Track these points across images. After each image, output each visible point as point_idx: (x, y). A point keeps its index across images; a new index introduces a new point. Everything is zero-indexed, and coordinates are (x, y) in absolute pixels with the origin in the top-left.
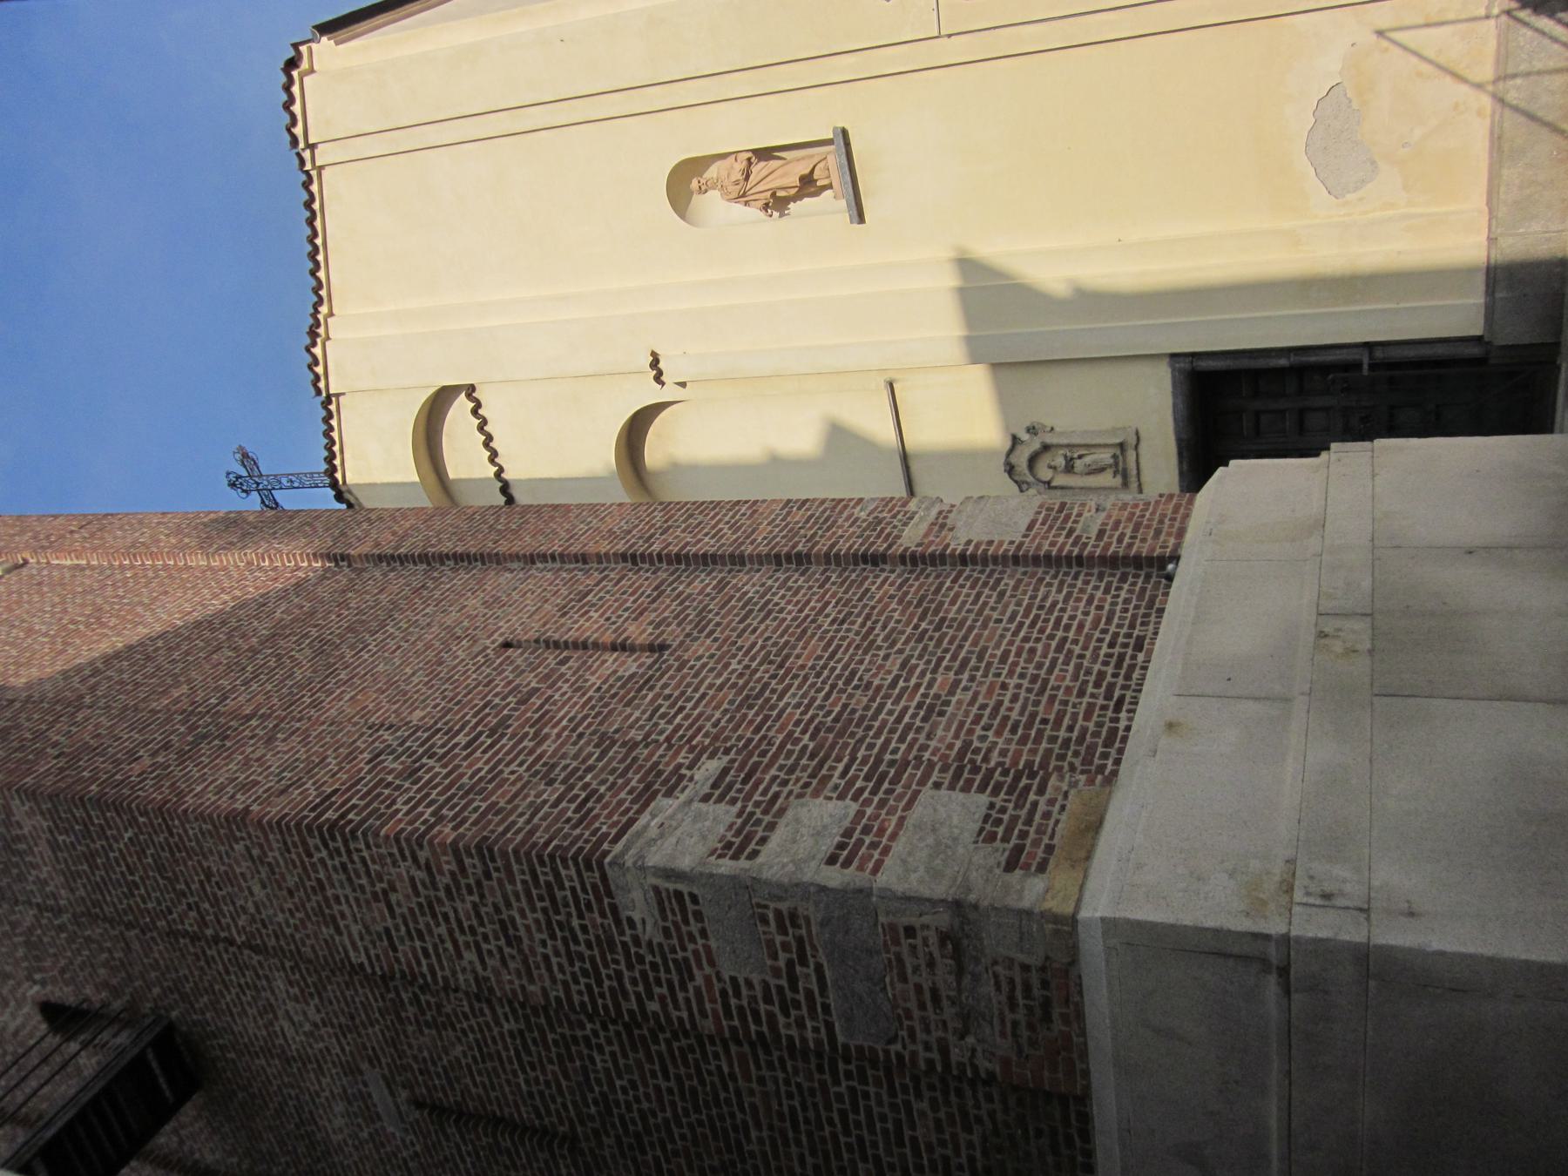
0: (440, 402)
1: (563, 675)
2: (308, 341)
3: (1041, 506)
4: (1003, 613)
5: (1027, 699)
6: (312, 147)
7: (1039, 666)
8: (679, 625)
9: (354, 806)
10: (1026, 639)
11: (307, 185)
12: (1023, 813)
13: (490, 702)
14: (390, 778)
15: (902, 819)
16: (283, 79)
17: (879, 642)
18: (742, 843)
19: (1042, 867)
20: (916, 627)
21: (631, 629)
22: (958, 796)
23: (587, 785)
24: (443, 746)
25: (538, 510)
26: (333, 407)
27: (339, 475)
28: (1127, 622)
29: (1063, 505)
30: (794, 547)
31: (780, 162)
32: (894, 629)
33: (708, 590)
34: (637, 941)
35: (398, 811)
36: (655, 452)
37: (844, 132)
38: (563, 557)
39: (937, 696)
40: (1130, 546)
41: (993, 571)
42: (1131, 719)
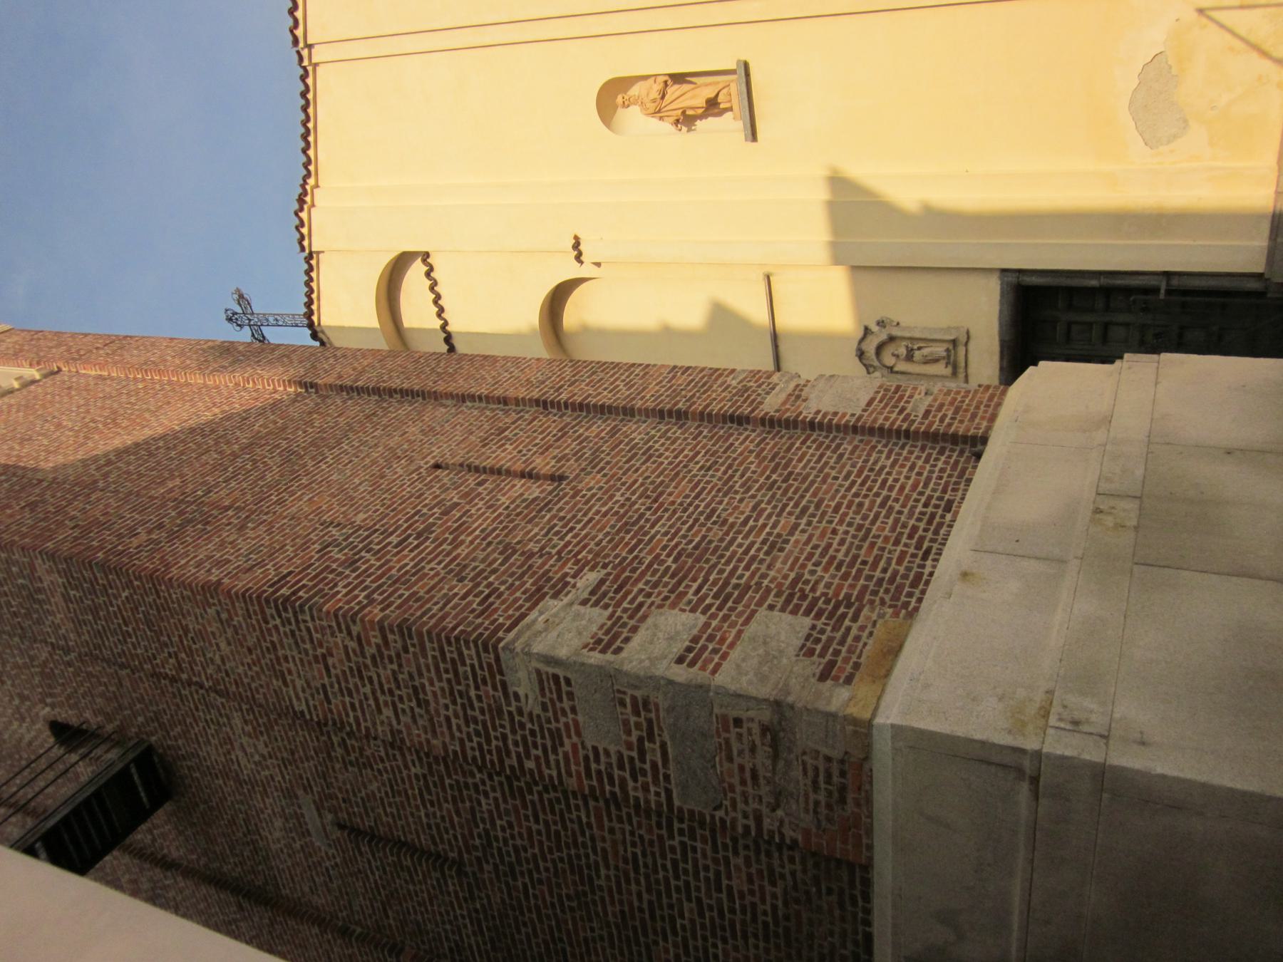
1: (480, 494)
2: (296, 206)
3: (880, 387)
4: (840, 472)
5: (852, 543)
6: (310, 47)
7: (865, 518)
8: (576, 461)
9: (304, 586)
10: (856, 495)
11: (303, 78)
12: (838, 635)
14: (334, 566)
15: (740, 632)
17: (737, 488)
18: (610, 640)
19: (849, 680)
20: (768, 478)
21: (538, 461)
22: (786, 617)
23: (490, 584)
24: (378, 543)
25: (472, 358)
26: (313, 262)
27: (315, 318)
29: (898, 388)
30: (676, 404)
32: (749, 478)
35: (338, 592)
36: (572, 316)
37: (746, 65)
38: (488, 399)
39: (779, 535)
40: (950, 425)
41: (835, 437)
42: (934, 567)
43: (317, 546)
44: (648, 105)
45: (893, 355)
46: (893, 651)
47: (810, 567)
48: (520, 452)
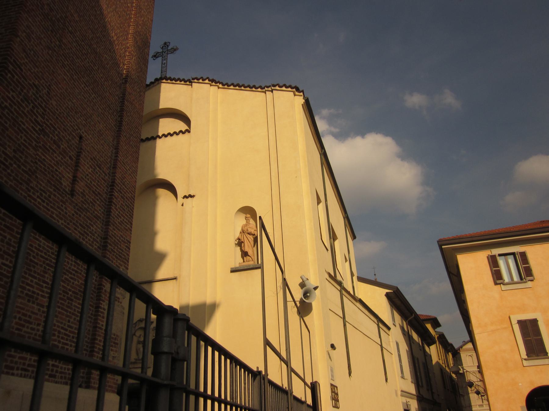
0: (186, 119)
1: (65, 158)
2: (211, 78)
3: (117, 336)
4: (72, 323)
5: (32, 334)
6: (272, 91)
8: (82, 201)
9: (14, 76)
11: (261, 87)
13: (56, 130)
14: (25, 91)
16: (293, 86)
20: (70, 290)
21: (82, 184)
23: (11, 165)
24: (37, 112)
25: (137, 152)
26: (188, 83)
27: (164, 81)
28: (63, 370)
30: (110, 245)
31: (253, 245)
32: (70, 282)
33: (96, 212)
35: (9, 93)
36: (162, 193)
38: (116, 160)
39: (37, 299)
41: (92, 318)
42: (17, 375)
43: (37, 83)
44: (246, 228)
45: (140, 335)
47: (18, 316)
48: (87, 175)
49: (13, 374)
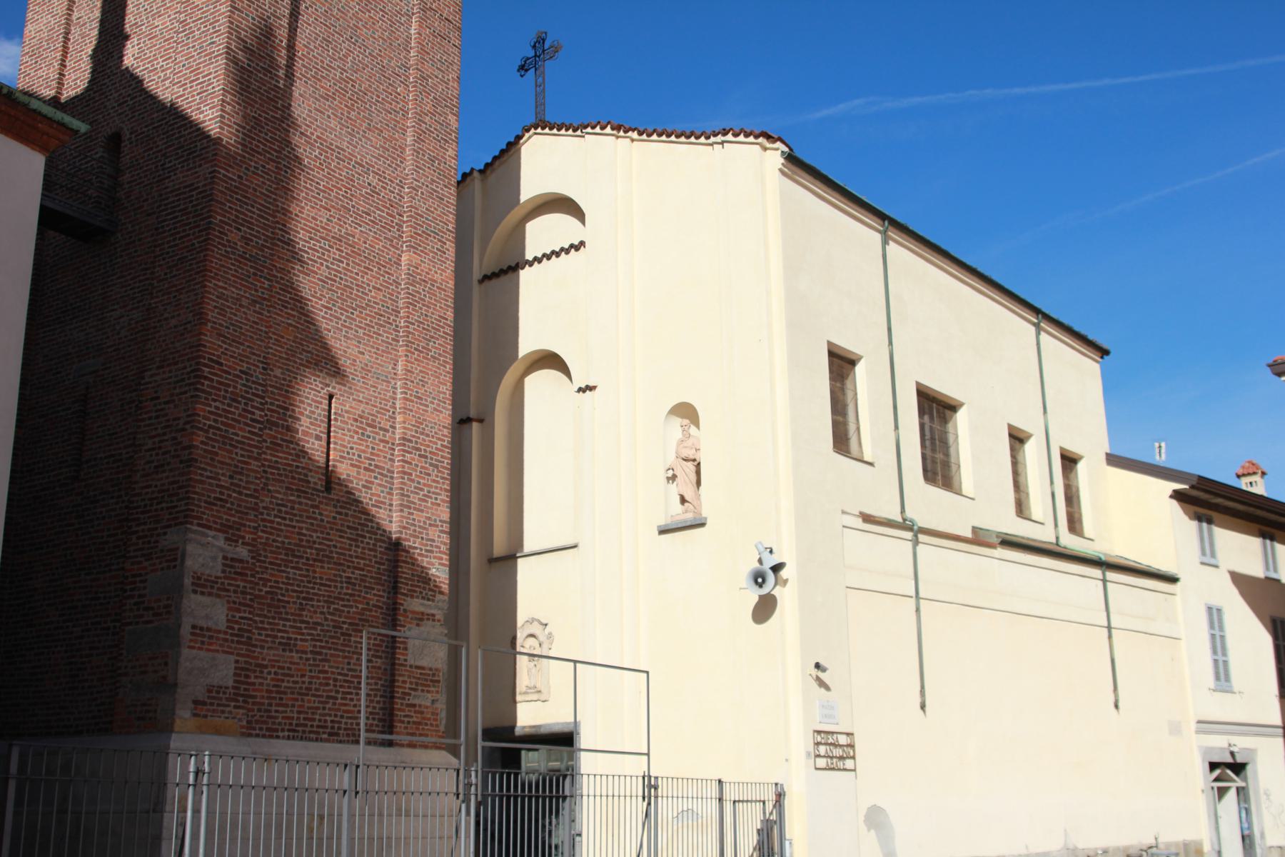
7: (317, 690)
10: (336, 680)
12: (224, 702)
15: (217, 651)
18: (202, 585)
19: (195, 715)
22: (232, 672)
34: (158, 535)
37: (703, 525)
40: (403, 722)
42: (283, 737)
46: (218, 731)
49: (278, 737)
